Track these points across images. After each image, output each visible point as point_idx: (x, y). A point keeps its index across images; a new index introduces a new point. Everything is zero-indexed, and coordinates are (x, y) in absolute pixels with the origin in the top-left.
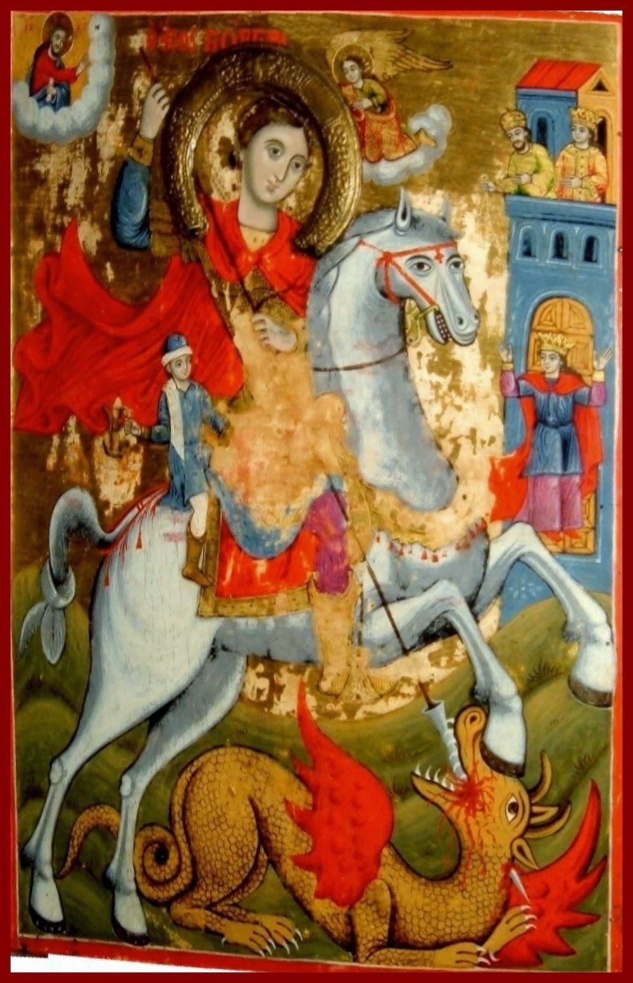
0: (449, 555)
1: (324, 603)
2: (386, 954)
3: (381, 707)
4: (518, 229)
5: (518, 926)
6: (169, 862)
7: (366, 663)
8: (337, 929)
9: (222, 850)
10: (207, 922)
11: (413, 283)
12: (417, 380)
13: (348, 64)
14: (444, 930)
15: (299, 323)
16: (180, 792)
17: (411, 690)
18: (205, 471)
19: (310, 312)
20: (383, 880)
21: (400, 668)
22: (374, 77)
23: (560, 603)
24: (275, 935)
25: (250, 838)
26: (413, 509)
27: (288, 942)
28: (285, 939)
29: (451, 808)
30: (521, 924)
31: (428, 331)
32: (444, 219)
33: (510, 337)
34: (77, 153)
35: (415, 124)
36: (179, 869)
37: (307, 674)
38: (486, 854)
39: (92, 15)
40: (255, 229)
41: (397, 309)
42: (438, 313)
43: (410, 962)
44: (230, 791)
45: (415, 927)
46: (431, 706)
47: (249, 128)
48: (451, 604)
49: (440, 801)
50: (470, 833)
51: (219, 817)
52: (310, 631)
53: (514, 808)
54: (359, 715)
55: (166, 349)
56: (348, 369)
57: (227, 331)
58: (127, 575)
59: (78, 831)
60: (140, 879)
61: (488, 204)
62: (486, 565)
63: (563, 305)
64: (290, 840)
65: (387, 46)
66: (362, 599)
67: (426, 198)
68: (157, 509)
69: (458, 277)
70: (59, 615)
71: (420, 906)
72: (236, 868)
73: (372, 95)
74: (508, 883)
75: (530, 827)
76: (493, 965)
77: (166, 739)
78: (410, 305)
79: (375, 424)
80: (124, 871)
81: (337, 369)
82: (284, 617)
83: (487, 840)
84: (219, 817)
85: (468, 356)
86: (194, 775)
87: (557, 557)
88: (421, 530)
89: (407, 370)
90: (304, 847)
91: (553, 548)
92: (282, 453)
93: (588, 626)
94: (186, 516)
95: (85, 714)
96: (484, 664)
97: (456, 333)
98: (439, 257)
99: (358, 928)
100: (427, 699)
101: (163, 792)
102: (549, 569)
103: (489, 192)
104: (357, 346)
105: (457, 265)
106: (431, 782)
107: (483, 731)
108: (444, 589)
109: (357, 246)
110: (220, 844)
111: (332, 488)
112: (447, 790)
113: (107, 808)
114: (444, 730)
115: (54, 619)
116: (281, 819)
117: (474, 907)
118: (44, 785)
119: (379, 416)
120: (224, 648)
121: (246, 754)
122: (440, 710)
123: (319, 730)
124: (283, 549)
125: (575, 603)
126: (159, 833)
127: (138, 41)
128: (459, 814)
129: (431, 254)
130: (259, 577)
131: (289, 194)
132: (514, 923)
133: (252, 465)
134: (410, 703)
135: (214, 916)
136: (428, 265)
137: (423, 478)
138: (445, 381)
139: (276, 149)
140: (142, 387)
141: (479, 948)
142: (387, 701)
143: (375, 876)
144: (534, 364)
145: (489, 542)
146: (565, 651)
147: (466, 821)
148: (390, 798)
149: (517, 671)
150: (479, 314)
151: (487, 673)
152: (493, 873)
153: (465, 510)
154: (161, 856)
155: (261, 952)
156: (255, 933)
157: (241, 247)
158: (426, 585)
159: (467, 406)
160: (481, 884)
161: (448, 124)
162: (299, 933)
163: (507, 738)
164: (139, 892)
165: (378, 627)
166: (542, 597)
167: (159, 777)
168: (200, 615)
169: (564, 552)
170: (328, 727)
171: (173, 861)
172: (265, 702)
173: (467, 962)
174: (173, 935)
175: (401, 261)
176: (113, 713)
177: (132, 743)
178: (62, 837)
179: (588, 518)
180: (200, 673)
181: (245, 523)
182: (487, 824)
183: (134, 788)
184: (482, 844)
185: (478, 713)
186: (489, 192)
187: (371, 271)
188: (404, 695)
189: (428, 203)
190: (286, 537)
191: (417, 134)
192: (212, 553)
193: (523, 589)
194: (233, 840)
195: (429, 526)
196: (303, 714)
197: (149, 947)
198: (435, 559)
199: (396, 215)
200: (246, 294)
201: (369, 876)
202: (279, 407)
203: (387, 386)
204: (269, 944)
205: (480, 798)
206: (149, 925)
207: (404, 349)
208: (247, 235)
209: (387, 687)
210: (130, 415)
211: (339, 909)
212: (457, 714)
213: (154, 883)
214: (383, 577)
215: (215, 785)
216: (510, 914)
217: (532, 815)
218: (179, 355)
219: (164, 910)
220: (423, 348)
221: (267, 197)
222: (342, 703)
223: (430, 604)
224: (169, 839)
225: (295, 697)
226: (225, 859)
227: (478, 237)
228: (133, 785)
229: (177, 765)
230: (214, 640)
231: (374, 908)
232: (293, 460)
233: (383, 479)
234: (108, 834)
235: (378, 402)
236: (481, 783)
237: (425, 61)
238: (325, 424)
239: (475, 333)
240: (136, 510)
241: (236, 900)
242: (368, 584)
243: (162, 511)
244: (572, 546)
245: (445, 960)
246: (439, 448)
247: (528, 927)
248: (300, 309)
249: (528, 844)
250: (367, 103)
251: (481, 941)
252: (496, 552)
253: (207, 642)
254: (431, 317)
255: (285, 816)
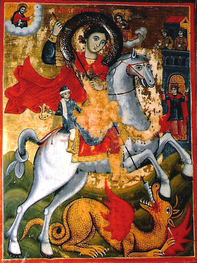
0: (149, 142)
1: (113, 157)
2: (135, 254)
3: (130, 184)
4: (165, 58)
5: (170, 244)
6: (61, 233)
7: (125, 172)
8: (118, 248)
9: (80, 228)
10: (75, 249)
11: (137, 72)
12: (139, 97)
13: (118, 17)
14: (150, 246)
15: (104, 83)
16: (65, 212)
17: (139, 179)
18: (74, 123)
19: (107, 80)
20: (132, 233)
21: (136, 173)
22: (125, 21)
23: (179, 154)
24: (97, 251)
25: (89, 224)
26: (138, 130)
27: (102, 253)
28: (101, 252)
29: (151, 211)
30: (171, 243)
31: (142, 84)
32: (145, 56)
33: (164, 85)
34: (30, 39)
35: (137, 32)
36: (65, 234)
37: (108, 176)
38: (161, 223)
39: (35, 4)
40: (90, 59)
41: (132, 80)
42: (144, 79)
43: (140, 256)
44: (83, 211)
45: (142, 245)
46: (145, 183)
47: (87, 35)
48: (150, 155)
49: (148, 210)
50: (156, 218)
51: (79, 218)
52: (108, 164)
53: (168, 210)
54: (124, 187)
55: (62, 90)
56: (118, 94)
57: (82, 85)
58: (47, 152)
59: (28, 227)
60: (51, 238)
61: (157, 52)
62: (159, 145)
63: (177, 76)
64: (102, 223)
65: (129, 13)
66: (124, 155)
67: (140, 51)
68: (58, 133)
69: (149, 70)
70: (22, 164)
71: (143, 240)
72: (85, 233)
73: (124, 25)
74: (167, 231)
75: (173, 216)
76: (164, 256)
77: (60, 197)
78: (136, 77)
79: (127, 108)
80: (45, 237)
81: (115, 94)
82: (100, 161)
83: (161, 219)
84: (79, 218)
85: (153, 90)
86: (70, 207)
87: (177, 141)
88: (141, 136)
89: (136, 94)
90: (107, 224)
91: (177, 139)
92: (99, 117)
93: (186, 159)
94: (68, 135)
95: (31, 192)
96: (159, 171)
97: (149, 84)
98: (144, 65)
99: (124, 247)
100: (143, 181)
101: (59, 213)
102: (176, 145)
103: (157, 49)
104: (122, 88)
105: (149, 67)
106: (145, 204)
107: (159, 190)
108: (147, 151)
109: (121, 62)
110: (80, 226)
111: (114, 126)
112: (150, 206)
113: (39, 219)
114: (148, 190)
115: (20, 165)
116: (99, 218)
117: (158, 239)
118: (15, 214)
119: (128, 106)
120: (81, 170)
121: (88, 200)
122: (147, 184)
123: (112, 192)
124: (100, 143)
125: (182, 153)
126: (58, 224)
127: (51, 11)
128: (153, 213)
129: (142, 64)
130: (92, 150)
131: (100, 50)
132: (169, 242)
133: (90, 121)
134: (139, 182)
135: (77, 247)
136: (141, 67)
137: (141, 122)
138: (147, 97)
139: (96, 38)
140: (53, 101)
141: (159, 251)
142: (132, 182)
143: (129, 232)
144: (170, 92)
145: (159, 138)
146: (180, 166)
147: (155, 214)
148: (133, 209)
149: (168, 172)
150: (156, 79)
151: (160, 173)
152: (163, 229)
153: (153, 130)
154: (59, 231)
155: (93, 257)
156: (91, 251)
157: (86, 63)
158: (142, 151)
159: (153, 102)
160: (160, 232)
161: (146, 32)
162: (106, 250)
163: (166, 191)
164: (50, 243)
165: (129, 162)
166: (174, 152)
167: (58, 208)
168: (72, 162)
169: (179, 140)
170: (114, 191)
171: (63, 232)
172: (94, 184)
173: (156, 255)
174: (62, 254)
175: (133, 66)
176: (41, 191)
177: (48, 199)
178: (21, 228)
179: (185, 131)
180: (73, 178)
181: (87, 136)
182: (161, 215)
183: (49, 213)
184: (160, 221)
185: (158, 184)
186: (157, 49)
187: (125, 69)
188: (136, 180)
189: (141, 52)
190: (100, 139)
191: (137, 34)
192: (76, 145)
193: (169, 150)
194: (84, 224)
195: (143, 135)
196: (106, 187)
197: (54, 258)
198: (145, 144)
199: (132, 55)
200: (87, 76)
201: (127, 231)
202: (98, 105)
203: (130, 99)
204: (96, 254)
205: (159, 208)
206: (54, 252)
207: (135, 89)
208: (87, 60)
209: (132, 178)
210: (49, 108)
211: (118, 242)
212: (151, 184)
213: (56, 239)
214: (130, 149)
215: (78, 209)
216: (168, 240)
217: (173, 212)
218: (66, 92)
219: (60, 247)
220: (140, 89)
221: (94, 51)
222: (118, 183)
223: (144, 155)
224: (62, 225)
225: (104, 183)
226: (81, 230)
227: (155, 60)
228: (49, 211)
229: (65, 204)
230: (78, 168)
231: (129, 241)
232: (102, 119)
233: (130, 123)
234: (39, 227)
235: (128, 103)
236: (159, 204)
237: (140, 16)
238: (112, 109)
239: (154, 84)
240: (51, 134)
241: (85, 242)
242: (125, 151)
243: (59, 134)
244: (181, 139)
245: (150, 255)
246: (145, 114)
247: (173, 243)
248: (104, 79)
249: (172, 220)
250: (123, 27)
251: (160, 248)
252: (161, 141)
253: (75, 169)
254: (142, 80)
255: (101, 217)
